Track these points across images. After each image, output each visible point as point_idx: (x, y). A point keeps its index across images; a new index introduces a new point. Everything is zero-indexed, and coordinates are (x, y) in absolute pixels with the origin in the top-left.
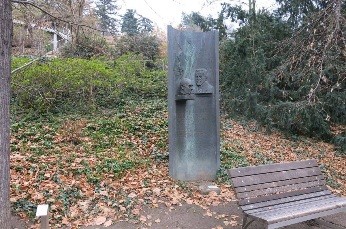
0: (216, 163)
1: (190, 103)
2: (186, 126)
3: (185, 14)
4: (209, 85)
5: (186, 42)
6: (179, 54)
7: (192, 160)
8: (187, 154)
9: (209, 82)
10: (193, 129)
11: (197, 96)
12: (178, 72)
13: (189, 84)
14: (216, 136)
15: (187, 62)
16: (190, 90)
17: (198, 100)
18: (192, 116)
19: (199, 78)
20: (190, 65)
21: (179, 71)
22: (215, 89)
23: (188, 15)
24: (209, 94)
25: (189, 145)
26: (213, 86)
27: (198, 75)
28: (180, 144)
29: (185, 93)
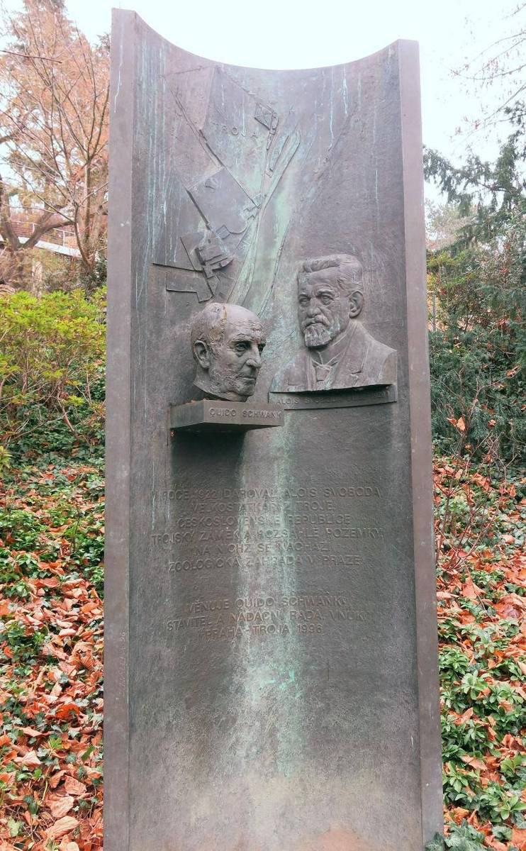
0: (419, 801)
1: (275, 442)
2: (246, 572)
3: (433, 203)
4: (374, 342)
5: (245, 119)
6: (203, 180)
7: (280, 769)
8: (246, 736)
9: (373, 328)
10: (288, 590)
11: (308, 402)
12: (195, 275)
13: (234, 336)
14: (414, 636)
15: (253, 224)
16: (246, 370)
17: (314, 423)
18: (280, 518)
19: (315, 306)
20: (269, 242)
21: (202, 272)
22: (403, 362)
23: (440, 207)
24: (371, 396)
25: (265, 678)
26: (392, 346)
27: (310, 287)
28: (203, 684)
29: (212, 389)
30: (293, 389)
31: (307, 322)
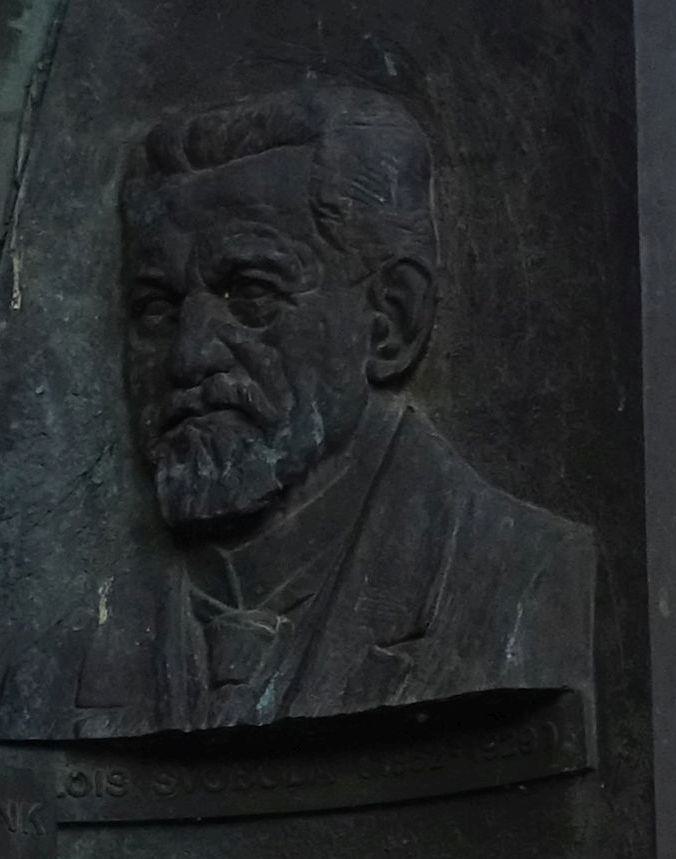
30: (99, 728)
31: (162, 407)
